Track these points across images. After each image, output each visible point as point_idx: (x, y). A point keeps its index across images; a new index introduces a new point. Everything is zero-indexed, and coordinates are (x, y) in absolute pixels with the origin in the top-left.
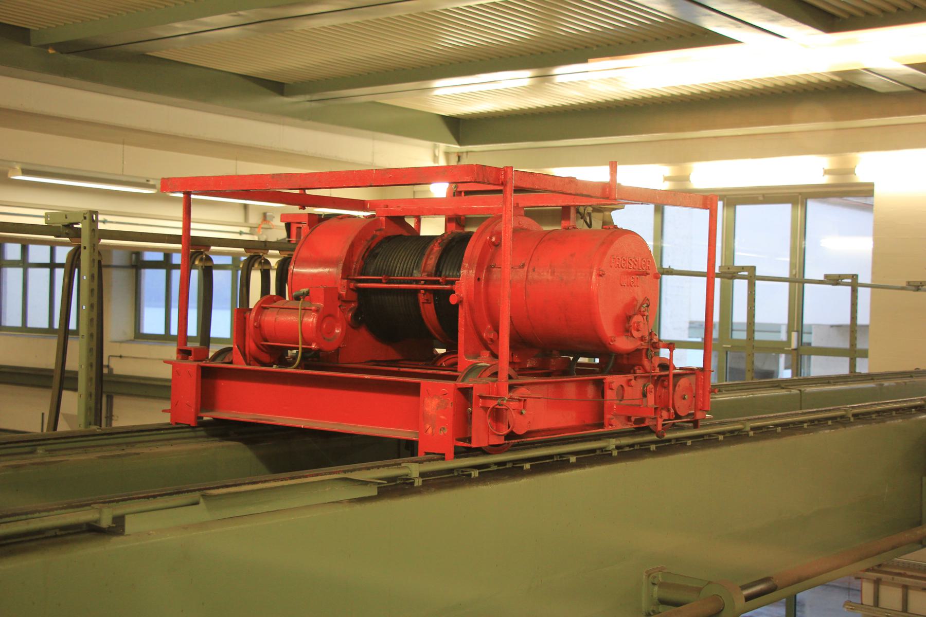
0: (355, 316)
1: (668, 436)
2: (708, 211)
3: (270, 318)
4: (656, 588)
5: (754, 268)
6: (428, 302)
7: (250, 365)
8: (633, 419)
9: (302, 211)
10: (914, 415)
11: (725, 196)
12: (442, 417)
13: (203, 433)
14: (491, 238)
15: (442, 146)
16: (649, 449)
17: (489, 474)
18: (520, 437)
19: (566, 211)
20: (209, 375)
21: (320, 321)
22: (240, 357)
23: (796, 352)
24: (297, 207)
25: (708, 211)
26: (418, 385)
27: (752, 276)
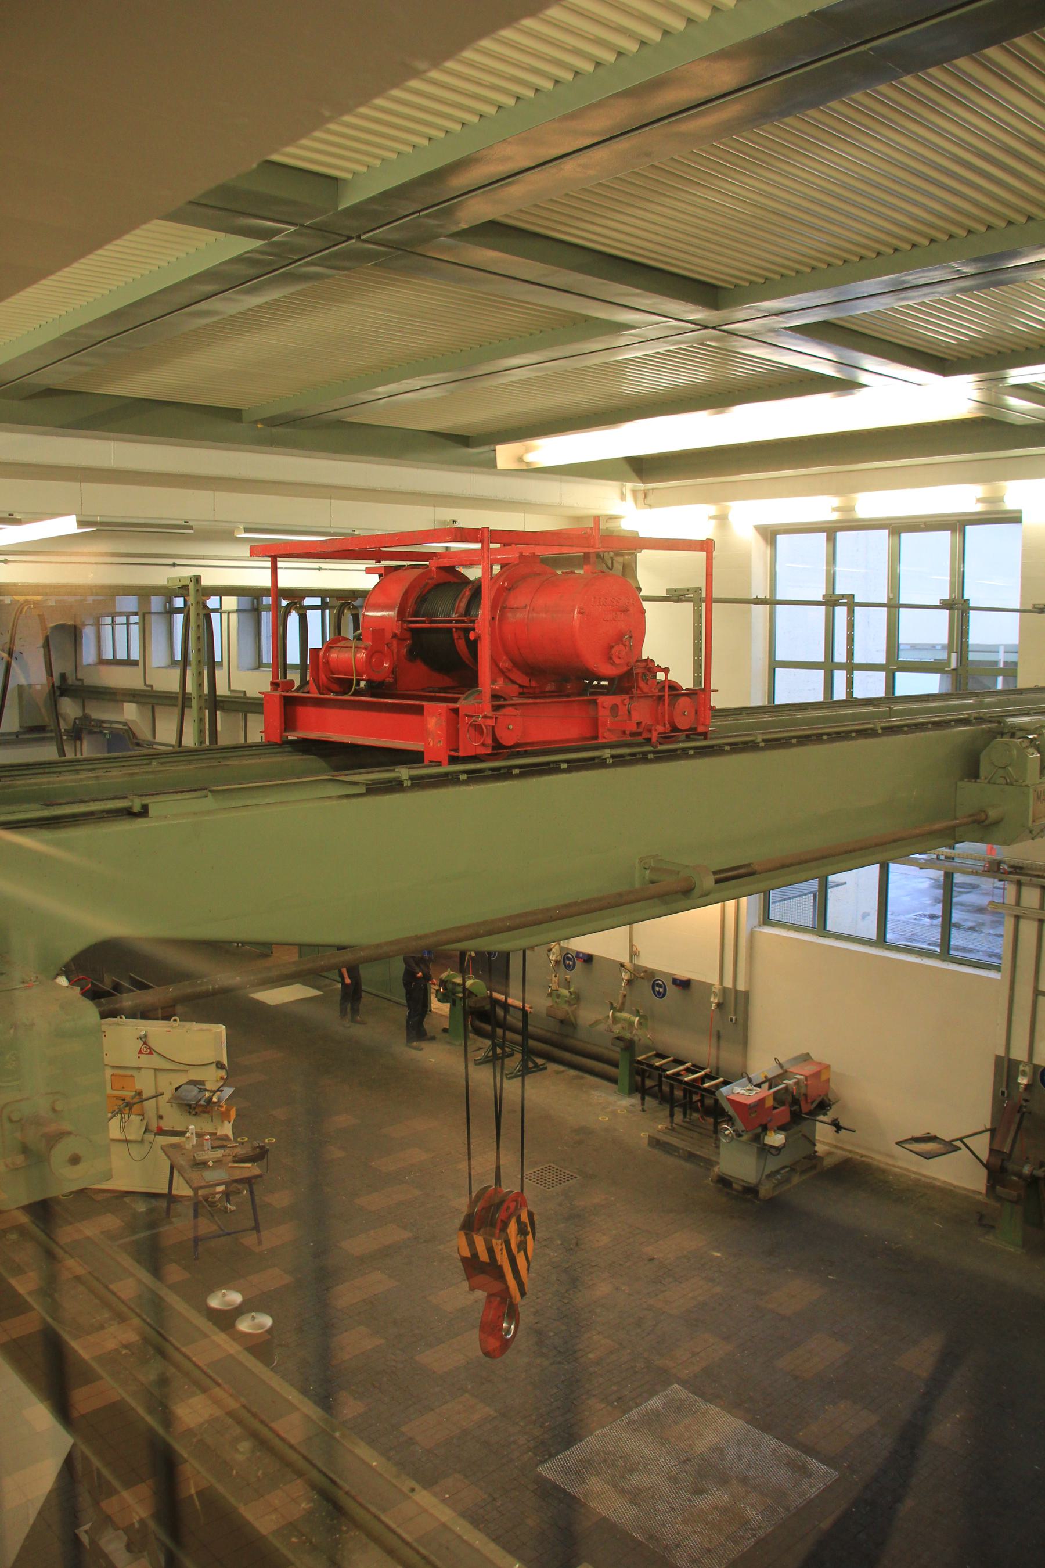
0: (410, 651)
1: (661, 747)
2: (705, 553)
3: (334, 655)
4: (647, 872)
5: (853, 596)
6: (460, 638)
7: (323, 694)
8: (628, 732)
9: (378, 565)
10: (953, 727)
11: (891, 524)
12: (439, 732)
13: (290, 749)
14: (503, 583)
15: (629, 486)
16: (647, 758)
17: (475, 777)
18: (506, 747)
19: (586, 557)
20: (290, 703)
21: (370, 657)
22: (315, 689)
23: (954, 672)
24: (374, 562)
25: (705, 553)
26: (421, 707)
27: (850, 603)
